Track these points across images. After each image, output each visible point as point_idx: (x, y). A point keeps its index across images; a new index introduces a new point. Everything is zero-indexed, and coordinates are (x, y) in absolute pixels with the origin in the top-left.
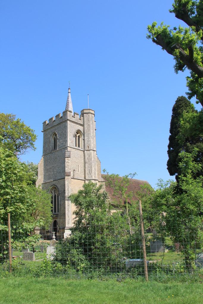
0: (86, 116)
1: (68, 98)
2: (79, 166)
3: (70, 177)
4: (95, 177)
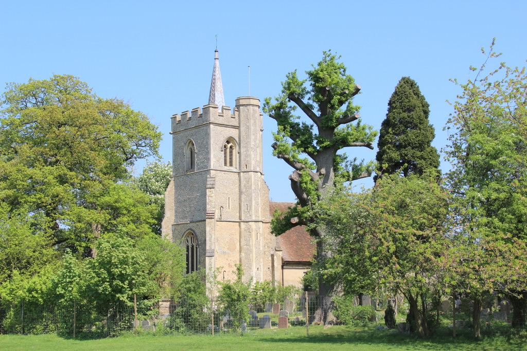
0: (244, 111)
1: (214, 71)
2: (230, 200)
3: (213, 219)
4: (256, 216)
